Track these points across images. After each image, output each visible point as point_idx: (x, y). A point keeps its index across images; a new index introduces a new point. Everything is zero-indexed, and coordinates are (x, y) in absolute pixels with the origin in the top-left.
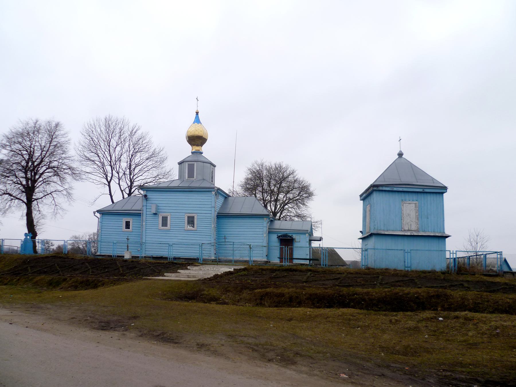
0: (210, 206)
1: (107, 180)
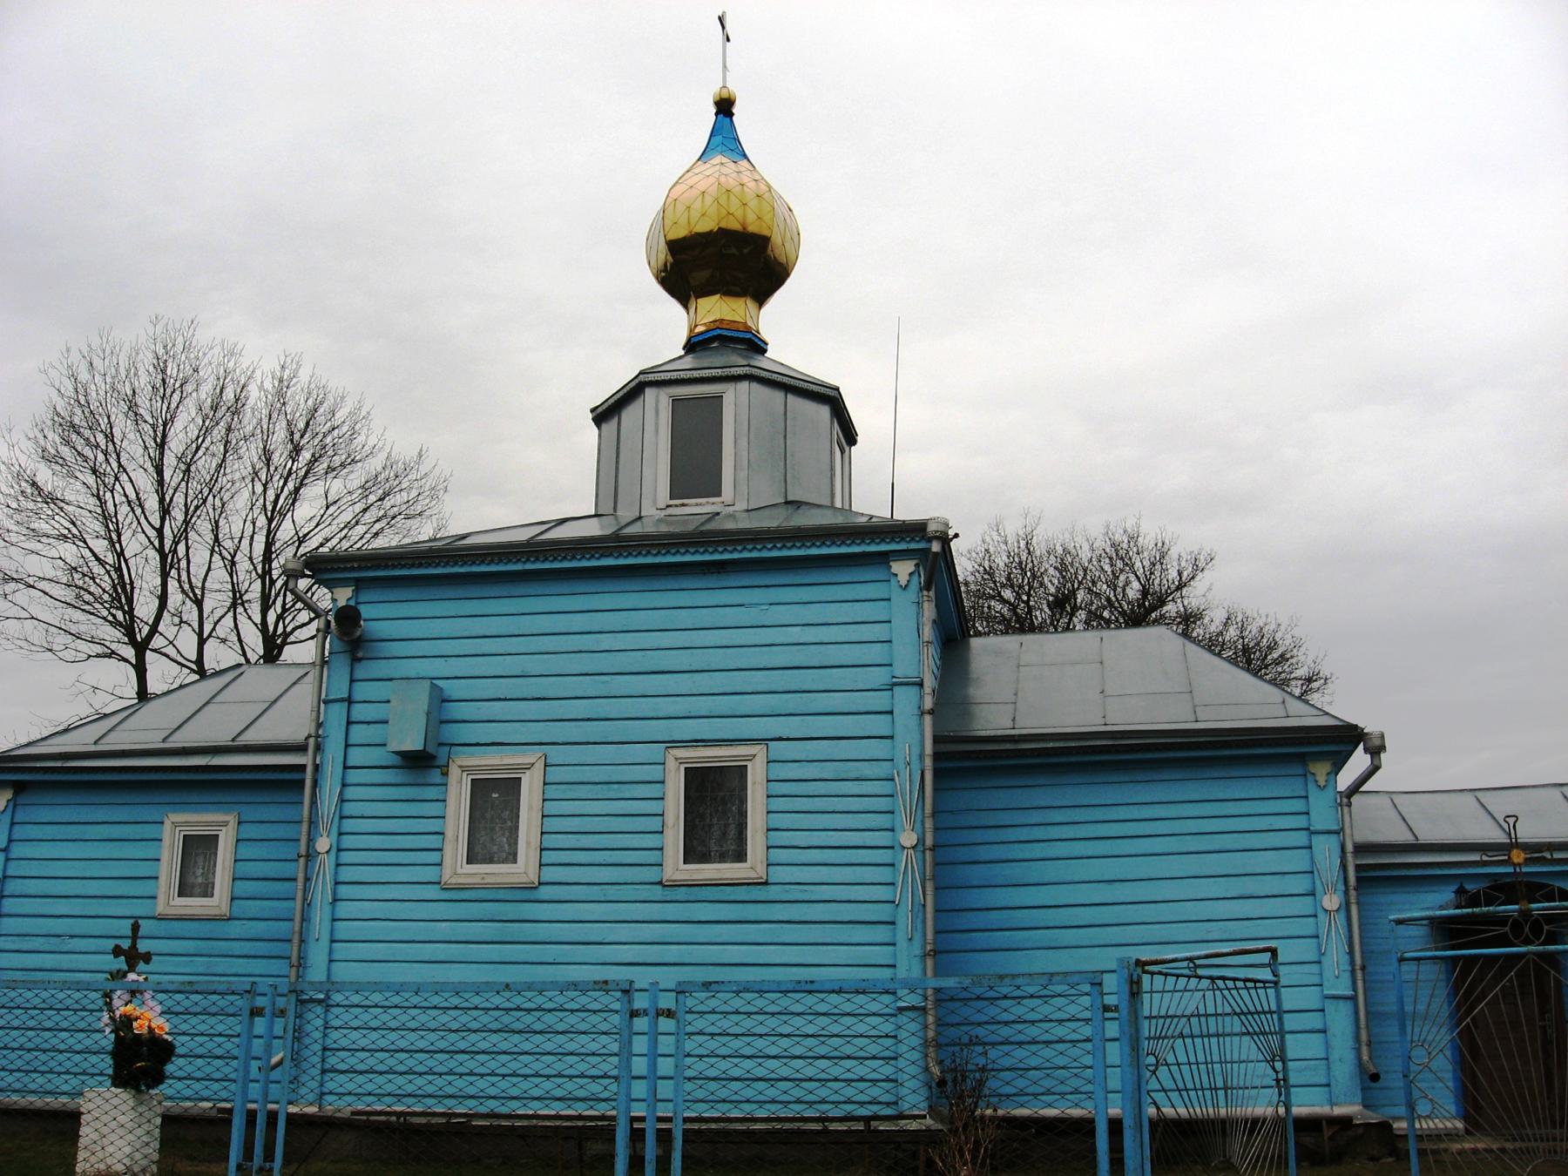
0: (880, 676)
1: (129, 631)
